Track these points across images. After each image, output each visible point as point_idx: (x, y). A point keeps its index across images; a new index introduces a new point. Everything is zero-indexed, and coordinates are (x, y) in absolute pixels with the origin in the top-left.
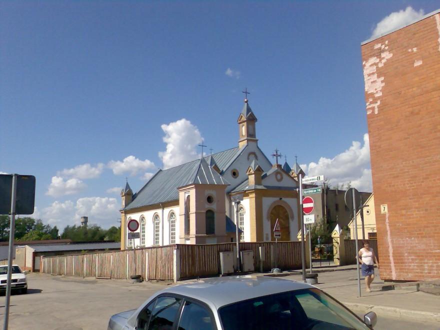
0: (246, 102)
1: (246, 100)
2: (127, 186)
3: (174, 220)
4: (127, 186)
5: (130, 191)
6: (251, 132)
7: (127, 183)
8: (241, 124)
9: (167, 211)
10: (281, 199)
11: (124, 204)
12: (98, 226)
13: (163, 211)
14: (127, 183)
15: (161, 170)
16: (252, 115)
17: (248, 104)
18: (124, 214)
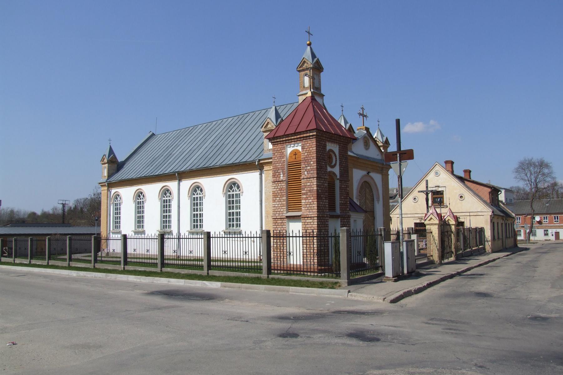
0: (310, 45)
1: (308, 42)
2: (111, 151)
3: (168, 198)
4: (111, 151)
5: (115, 157)
6: (317, 85)
7: (110, 146)
8: (303, 73)
9: (187, 184)
10: (368, 173)
11: (106, 174)
12: (530, 158)
13: (261, 174)
14: (110, 146)
15: (153, 134)
16: (318, 62)
17: (311, 48)
18: (106, 188)
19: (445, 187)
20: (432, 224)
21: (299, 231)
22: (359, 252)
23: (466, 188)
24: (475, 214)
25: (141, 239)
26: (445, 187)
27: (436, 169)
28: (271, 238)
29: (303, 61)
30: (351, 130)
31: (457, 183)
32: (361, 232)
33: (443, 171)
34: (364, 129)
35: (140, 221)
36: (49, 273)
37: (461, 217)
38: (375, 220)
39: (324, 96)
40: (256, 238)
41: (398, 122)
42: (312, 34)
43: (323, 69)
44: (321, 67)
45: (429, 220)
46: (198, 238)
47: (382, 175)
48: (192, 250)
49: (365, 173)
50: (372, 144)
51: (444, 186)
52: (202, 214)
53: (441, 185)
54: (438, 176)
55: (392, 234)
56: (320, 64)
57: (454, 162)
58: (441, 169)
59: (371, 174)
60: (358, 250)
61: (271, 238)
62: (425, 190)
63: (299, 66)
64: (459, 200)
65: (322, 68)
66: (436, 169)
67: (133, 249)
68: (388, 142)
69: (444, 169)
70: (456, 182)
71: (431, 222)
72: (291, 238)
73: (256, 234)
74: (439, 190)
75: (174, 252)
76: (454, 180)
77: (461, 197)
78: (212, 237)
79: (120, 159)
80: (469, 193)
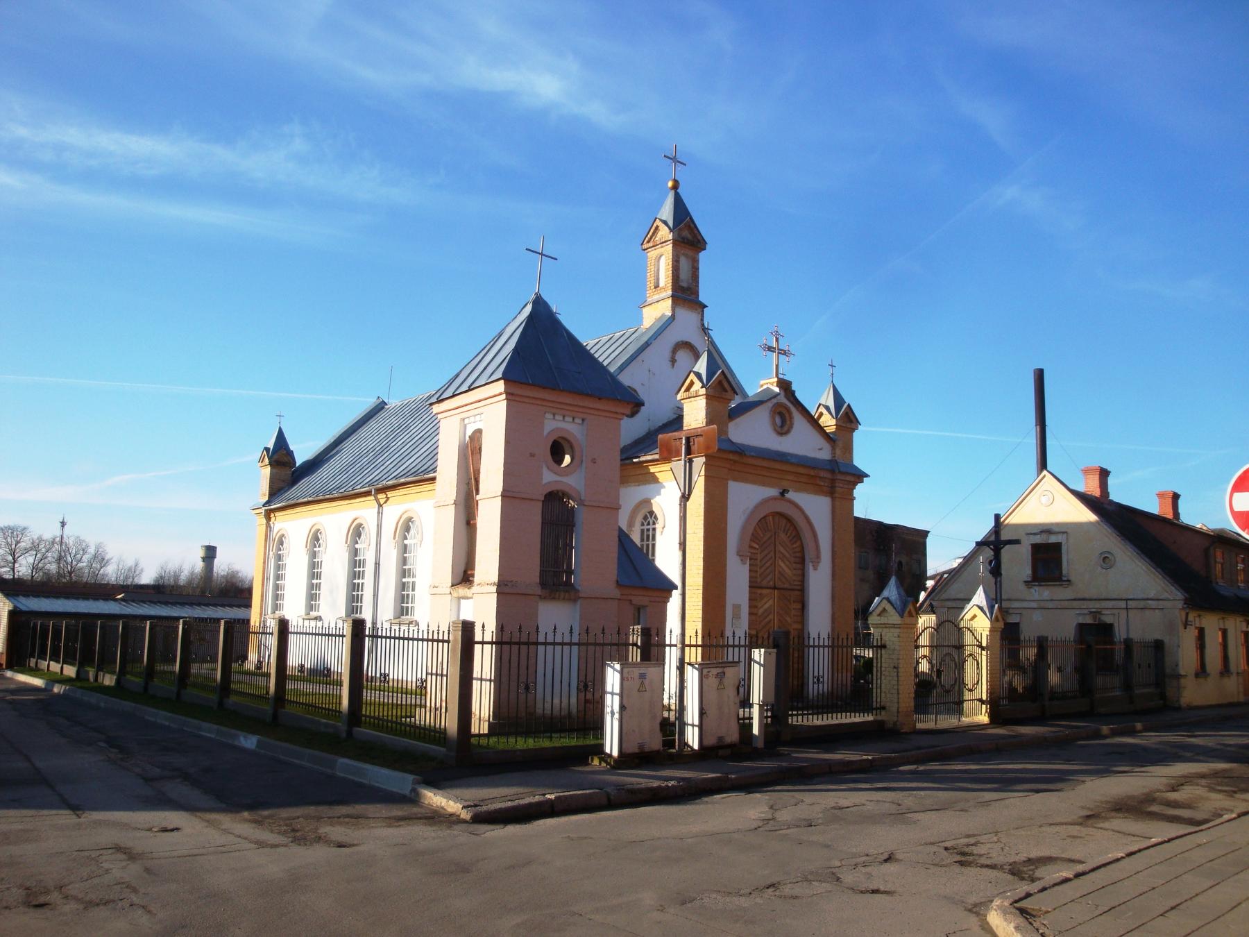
2: (281, 437)
4: (281, 437)
10: (783, 493)
19: (1066, 532)
20: (886, 626)
21: (697, 633)
25: (438, 641)
26: (1065, 535)
27: (1045, 488)
28: (476, 646)
29: (655, 225)
30: (726, 385)
32: (850, 639)
34: (775, 384)
35: (313, 595)
37: (1104, 612)
38: (806, 610)
39: (706, 306)
40: (552, 647)
41: (1040, 376)
42: (685, 162)
43: (706, 243)
44: (699, 238)
45: (879, 615)
46: (566, 644)
47: (833, 499)
48: (821, 674)
49: (772, 492)
50: (798, 418)
52: (363, 583)
55: (252, 633)
56: (696, 232)
59: (791, 495)
61: (476, 646)
63: (647, 239)
64: (1099, 568)
65: (702, 241)
66: (1045, 488)
67: (814, 677)
68: (852, 417)
71: (883, 620)
72: (730, 649)
73: (555, 632)
74: (1050, 542)
75: (815, 680)
78: (699, 646)
79: (302, 452)
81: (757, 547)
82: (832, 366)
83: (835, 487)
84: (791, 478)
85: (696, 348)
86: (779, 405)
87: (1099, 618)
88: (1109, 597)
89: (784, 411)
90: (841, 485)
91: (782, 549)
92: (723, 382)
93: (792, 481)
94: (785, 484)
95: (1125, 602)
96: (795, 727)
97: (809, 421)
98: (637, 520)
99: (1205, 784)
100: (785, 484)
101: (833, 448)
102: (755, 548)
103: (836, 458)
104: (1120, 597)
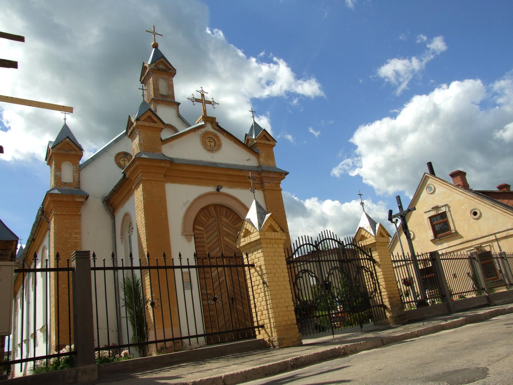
22: (455, 278)
23: (478, 198)
24: (504, 234)
31: (463, 194)
33: (438, 183)
36: (481, 270)
41: (162, 35)
44: (171, 67)
47: (264, 191)
49: (211, 189)
51: (444, 204)
53: (440, 204)
54: (432, 192)
57: (466, 173)
58: (434, 181)
59: (225, 190)
60: (456, 278)
62: (399, 212)
64: (472, 219)
69: (453, 187)
70: (461, 193)
76: (457, 191)
77: (475, 214)
80: (484, 204)
81: (203, 229)
82: (360, 195)
83: (264, 182)
84: (225, 179)
85: (175, 127)
86: (207, 133)
87: (481, 250)
88: (484, 235)
89: (212, 136)
90: (267, 181)
91: (226, 230)
92: (152, 117)
93: (227, 181)
94: (220, 183)
95: (494, 236)
96: (13, 300)
97: (235, 142)
98: (146, 243)
99: (441, 209)
100: (220, 183)
101: (258, 158)
102: (201, 230)
103: (261, 164)
104: (490, 233)
